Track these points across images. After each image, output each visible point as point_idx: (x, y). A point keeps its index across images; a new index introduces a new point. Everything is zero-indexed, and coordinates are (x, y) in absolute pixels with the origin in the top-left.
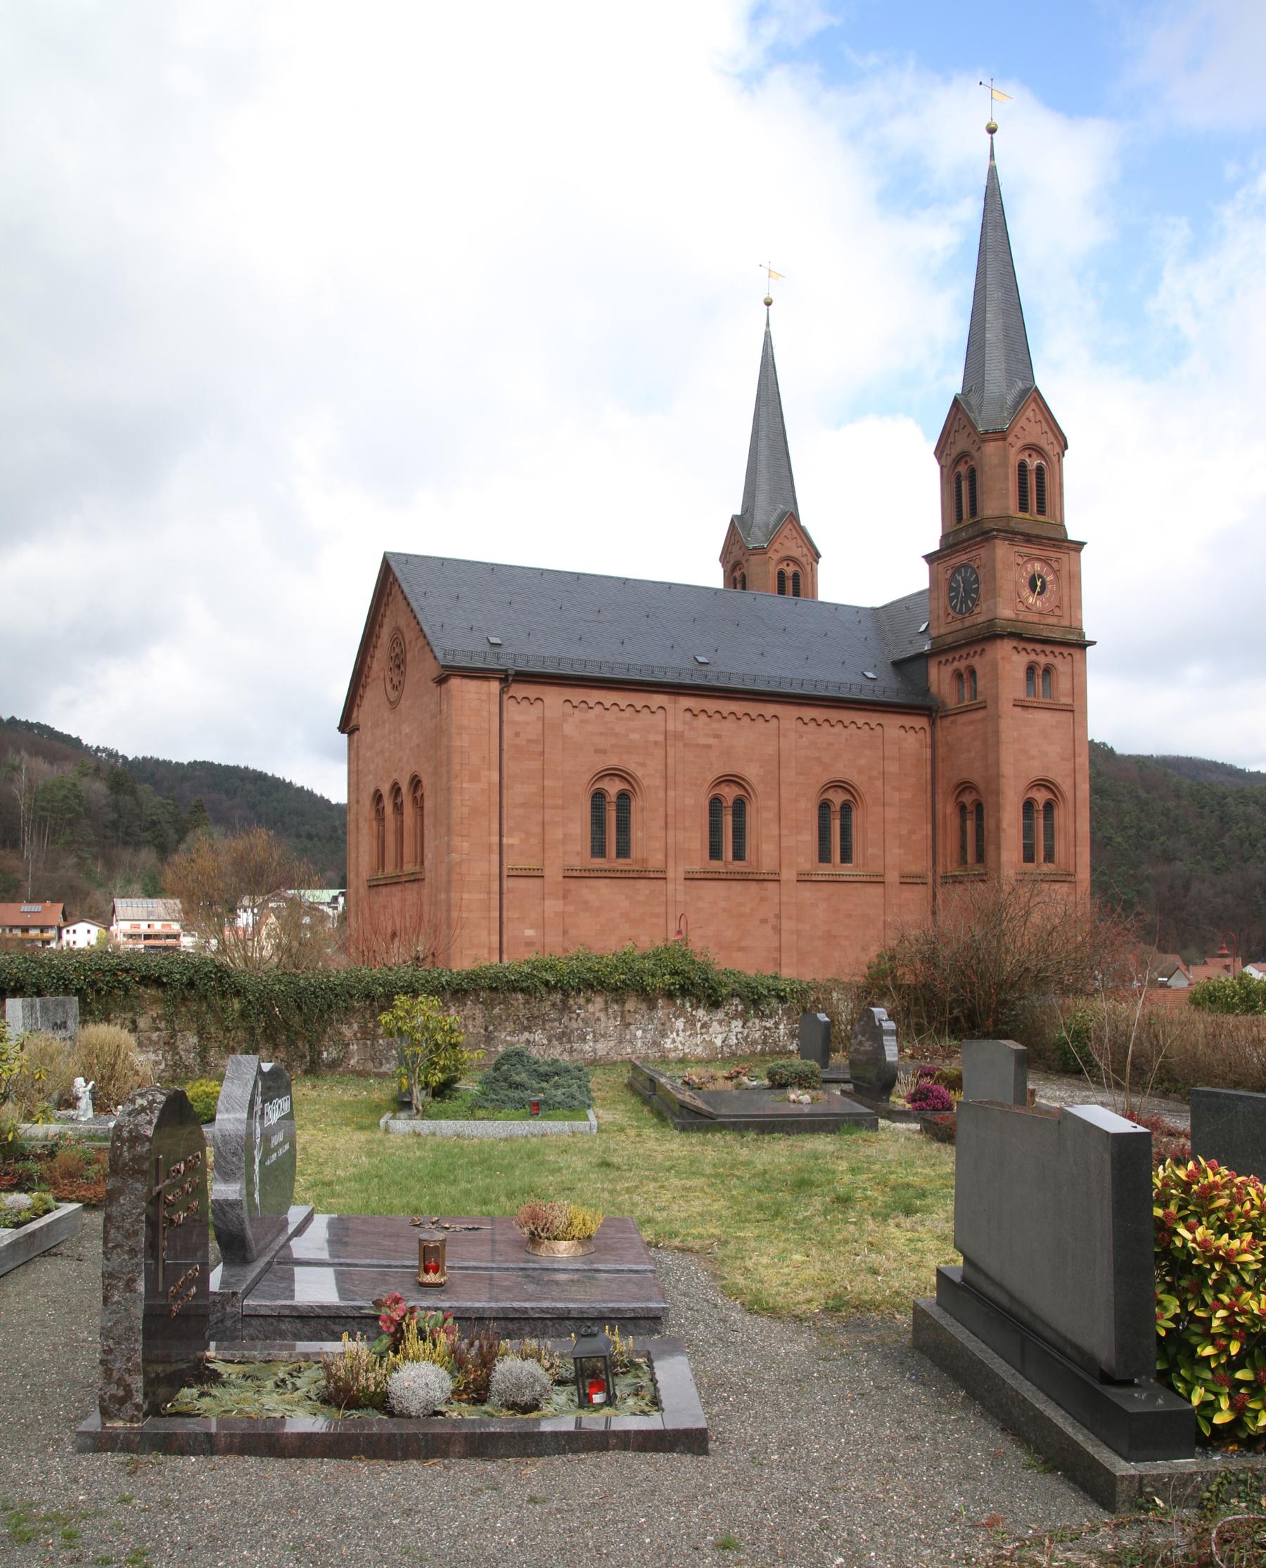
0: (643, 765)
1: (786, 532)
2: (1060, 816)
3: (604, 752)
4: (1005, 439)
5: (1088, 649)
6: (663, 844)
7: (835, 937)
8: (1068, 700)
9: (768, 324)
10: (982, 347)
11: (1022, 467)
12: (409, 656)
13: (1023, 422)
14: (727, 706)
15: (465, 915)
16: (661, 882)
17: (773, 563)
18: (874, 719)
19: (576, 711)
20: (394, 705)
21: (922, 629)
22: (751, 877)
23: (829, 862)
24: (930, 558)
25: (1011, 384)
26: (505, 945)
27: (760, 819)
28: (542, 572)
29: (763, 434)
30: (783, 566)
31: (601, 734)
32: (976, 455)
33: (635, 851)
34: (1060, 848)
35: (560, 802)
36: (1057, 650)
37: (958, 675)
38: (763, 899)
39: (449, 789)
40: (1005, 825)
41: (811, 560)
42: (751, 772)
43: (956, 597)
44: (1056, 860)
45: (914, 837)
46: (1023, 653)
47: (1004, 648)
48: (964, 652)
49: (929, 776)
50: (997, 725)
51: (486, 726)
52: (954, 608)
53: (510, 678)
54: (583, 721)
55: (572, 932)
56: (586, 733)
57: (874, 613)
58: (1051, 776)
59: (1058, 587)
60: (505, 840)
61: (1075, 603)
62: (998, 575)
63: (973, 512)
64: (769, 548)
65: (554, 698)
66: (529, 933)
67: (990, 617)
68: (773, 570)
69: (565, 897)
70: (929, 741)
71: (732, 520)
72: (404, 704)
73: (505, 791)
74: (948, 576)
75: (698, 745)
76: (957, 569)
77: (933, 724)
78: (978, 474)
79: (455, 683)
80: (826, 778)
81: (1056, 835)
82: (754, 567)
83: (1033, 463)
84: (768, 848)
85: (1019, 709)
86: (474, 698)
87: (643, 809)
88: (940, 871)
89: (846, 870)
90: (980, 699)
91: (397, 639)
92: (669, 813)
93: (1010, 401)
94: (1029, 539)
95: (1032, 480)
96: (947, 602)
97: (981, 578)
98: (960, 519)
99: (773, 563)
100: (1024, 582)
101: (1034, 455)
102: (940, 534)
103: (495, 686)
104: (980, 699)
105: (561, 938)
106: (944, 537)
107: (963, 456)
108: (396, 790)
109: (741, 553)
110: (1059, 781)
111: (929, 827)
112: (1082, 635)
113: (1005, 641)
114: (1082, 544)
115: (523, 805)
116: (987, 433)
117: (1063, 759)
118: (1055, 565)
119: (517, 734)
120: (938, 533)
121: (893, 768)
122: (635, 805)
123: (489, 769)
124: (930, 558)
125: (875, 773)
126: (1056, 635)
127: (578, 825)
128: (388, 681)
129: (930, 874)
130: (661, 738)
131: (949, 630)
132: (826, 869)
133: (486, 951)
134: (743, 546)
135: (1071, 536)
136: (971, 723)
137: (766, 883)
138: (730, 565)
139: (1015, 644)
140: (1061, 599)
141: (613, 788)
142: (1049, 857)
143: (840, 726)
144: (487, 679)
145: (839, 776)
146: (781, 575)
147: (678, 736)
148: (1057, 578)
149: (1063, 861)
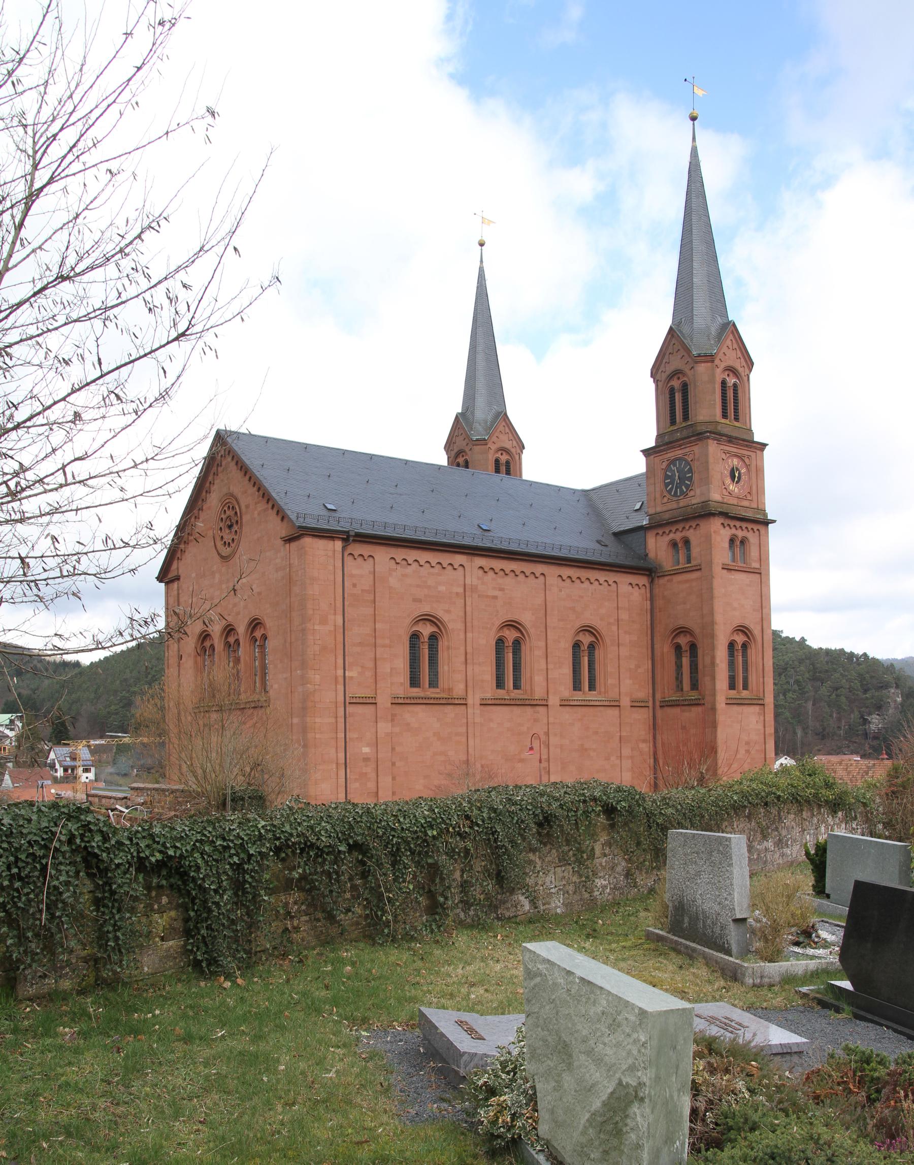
0: (448, 612)
1: (501, 428)
2: (752, 653)
3: (420, 601)
4: (713, 362)
6: (464, 676)
7: (586, 750)
8: (755, 565)
9: (482, 261)
10: (691, 287)
11: (724, 383)
12: (245, 518)
13: (724, 349)
14: (509, 566)
15: (317, 736)
16: (464, 707)
17: (492, 452)
18: (612, 577)
19: (399, 567)
21: (637, 507)
22: (527, 702)
24: (647, 452)
25: (713, 319)
26: (348, 761)
27: (533, 656)
28: (344, 452)
29: (480, 348)
31: (418, 586)
33: (443, 681)
35: (387, 642)
36: (750, 526)
37: (674, 544)
38: (536, 720)
39: (303, 630)
40: (718, 661)
41: (519, 451)
42: (526, 619)
44: (750, 687)
45: (639, 670)
46: (727, 528)
47: (716, 524)
48: (680, 526)
49: (649, 623)
50: (712, 584)
51: (332, 577)
52: (670, 492)
53: (351, 538)
56: (409, 586)
57: (586, 493)
58: (747, 623)
59: (750, 478)
60: (347, 674)
61: (760, 491)
63: (686, 417)
64: (483, 439)
65: (382, 555)
66: (366, 750)
67: (703, 499)
68: (491, 458)
70: (648, 595)
75: (487, 596)
76: (672, 462)
77: (652, 582)
78: (691, 389)
79: (307, 541)
80: (578, 624)
81: (750, 669)
82: (475, 455)
83: (731, 381)
84: (539, 679)
85: (725, 571)
86: (322, 554)
87: (448, 648)
88: (658, 696)
89: (592, 696)
90: (693, 563)
91: (230, 505)
93: (714, 330)
94: (731, 440)
95: (730, 394)
96: (663, 487)
97: (695, 469)
98: (673, 422)
99: (492, 452)
101: (731, 374)
102: (655, 434)
103: (339, 544)
104: (693, 563)
106: (659, 436)
107: (677, 373)
108: (229, 630)
109: (464, 443)
110: (752, 627)
111: (650, 662)
112: (765, 515)
113: (716, 518)
114: (765, 445)
115: (360, 644)
116: (699, 356)
117: (754, 610)
118: (747, 460)
119: (354, 585)
120: (654, 433)
121: (624, 616)
122: (442, 644)
123: (335, 614)
124: (647, 452)
125: (612, 620)
126: (749, 514)
127: (398, 662)
128: (218, 539)
129: (651, 699)
130: (461, 590)
131: (665, 509)
132: (578, 696)
133: (334, 766)
134: (468, 437)
136: (686, 581)
137: (538, 708)
138: (453, 453)
141: (426, 630)
142: (745, 687)
143: (587, 583)
144: (332, 538)
146: (497, 461)
147: (474, 589)
148: (748, 470)
149: (755, 689)
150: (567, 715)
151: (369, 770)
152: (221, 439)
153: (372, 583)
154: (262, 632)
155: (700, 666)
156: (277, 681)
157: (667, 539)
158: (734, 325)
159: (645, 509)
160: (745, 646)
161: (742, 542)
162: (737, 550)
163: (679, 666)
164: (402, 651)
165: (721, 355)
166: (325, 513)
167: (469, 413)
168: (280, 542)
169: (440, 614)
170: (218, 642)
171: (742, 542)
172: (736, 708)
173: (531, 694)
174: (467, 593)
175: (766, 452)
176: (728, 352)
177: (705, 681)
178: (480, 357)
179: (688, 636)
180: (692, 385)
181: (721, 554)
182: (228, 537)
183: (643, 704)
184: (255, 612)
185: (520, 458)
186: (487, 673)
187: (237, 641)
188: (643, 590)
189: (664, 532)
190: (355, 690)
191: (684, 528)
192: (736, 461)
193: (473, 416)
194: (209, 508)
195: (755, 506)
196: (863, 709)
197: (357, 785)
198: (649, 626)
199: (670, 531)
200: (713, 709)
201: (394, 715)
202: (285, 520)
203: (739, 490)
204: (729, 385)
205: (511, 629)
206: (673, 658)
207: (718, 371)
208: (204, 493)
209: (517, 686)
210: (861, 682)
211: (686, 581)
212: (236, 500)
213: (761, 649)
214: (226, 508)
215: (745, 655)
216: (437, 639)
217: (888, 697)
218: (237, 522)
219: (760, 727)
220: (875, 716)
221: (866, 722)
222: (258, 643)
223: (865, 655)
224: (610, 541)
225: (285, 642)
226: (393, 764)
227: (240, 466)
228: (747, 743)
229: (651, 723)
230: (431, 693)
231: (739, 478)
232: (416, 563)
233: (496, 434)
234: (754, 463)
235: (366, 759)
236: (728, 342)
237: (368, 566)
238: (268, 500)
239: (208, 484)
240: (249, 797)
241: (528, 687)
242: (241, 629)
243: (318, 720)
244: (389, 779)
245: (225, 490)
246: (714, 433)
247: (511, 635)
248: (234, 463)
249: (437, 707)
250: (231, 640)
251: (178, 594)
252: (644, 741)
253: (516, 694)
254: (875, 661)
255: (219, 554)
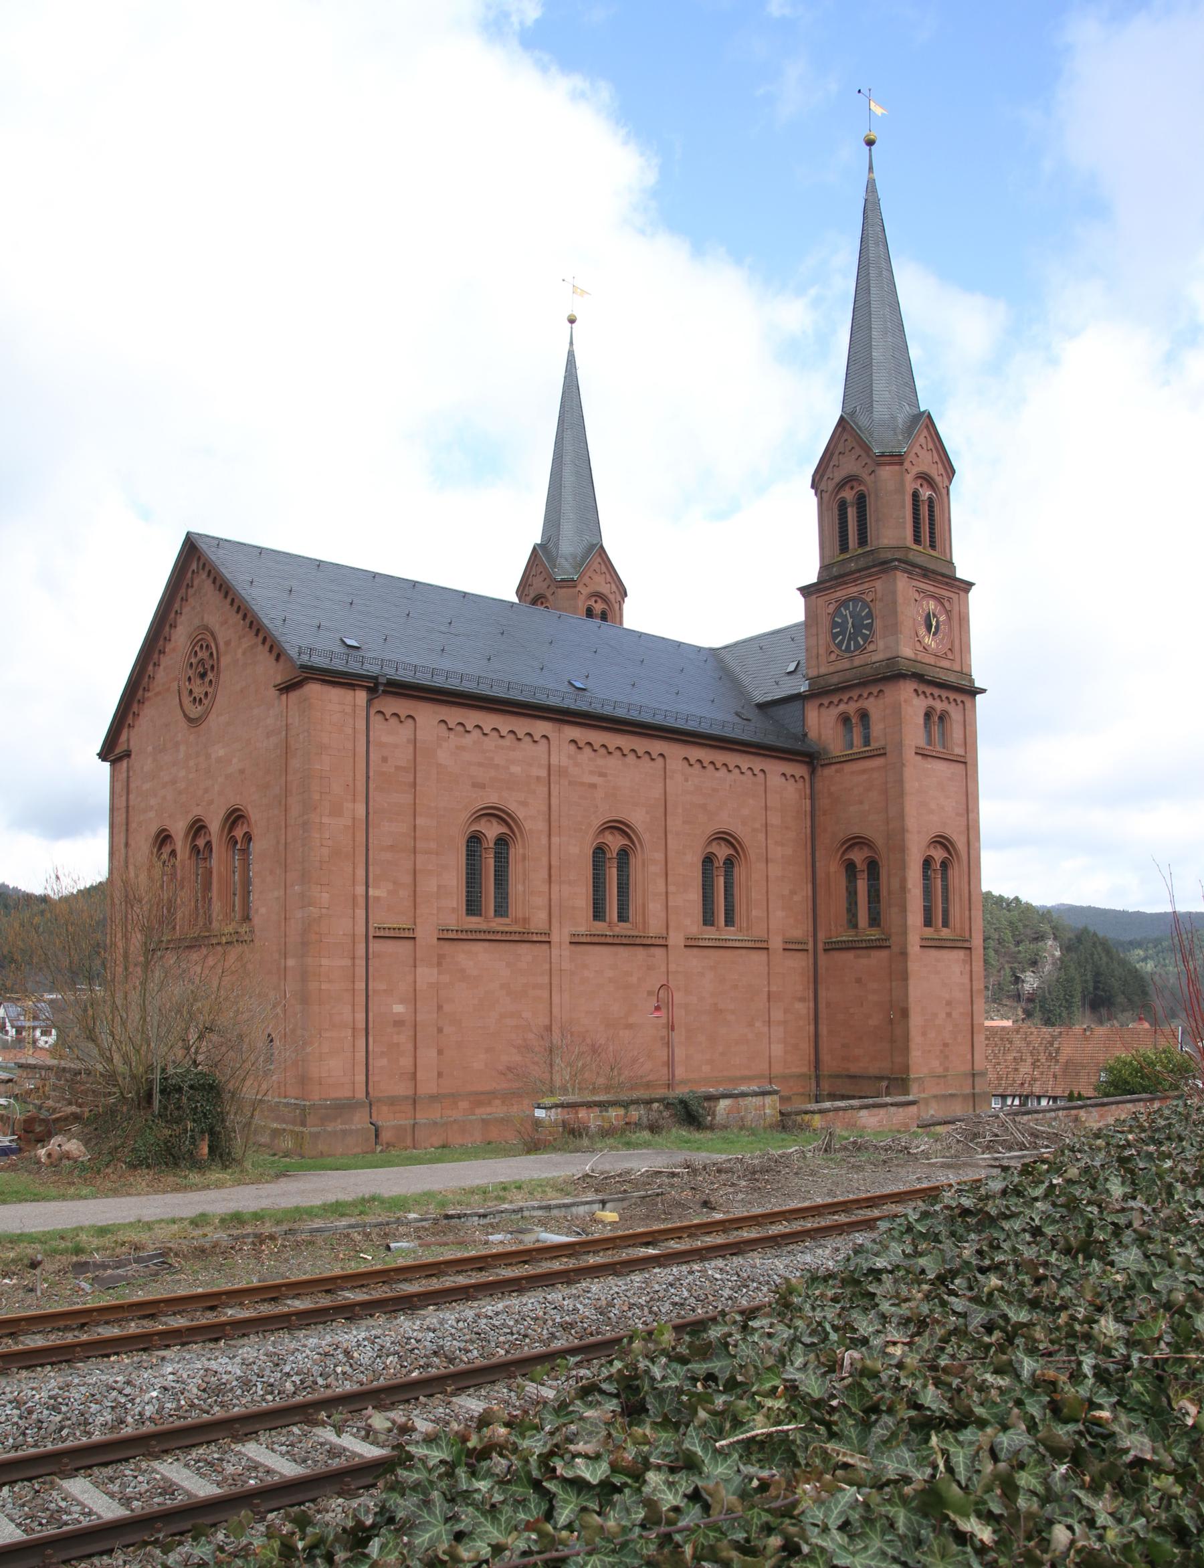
0: (524, 804)
1: (596, 566)
4: (901, 464)
5: (978, 697)
8: (959, 751)
9: (571, 343)
11: (915, 495)
12: (224, 661)
13: (917, 449)
16: (546, 946)
17: (582, 598)
20: (193, 722)
21: (791, 668)
22: (638, 941)
23: (712, 925)
24: (806, 591)
26: (371, 1025)
29: (567, 459)
30: (591, 602)
31: (480, 764)
32: (869, 479)
33: (517, 907)
34: (955, 911)
35: (433, 845)
37: (845, 719)
40: (910, 885)
41: (619, 598)
42: (637, 818)
43: (842, 633)
45: (796, 898)
46: (922, 697)
47: (907, 689)
48: (854, 694)
49: (809, 830)
50: (901, 774)
52: (839, 646)
54: (461, 748)
55: (447, 1008)
57: (713, 651)
59: (950, 627)
62: (899, 609)
63: (863, 540)
65: (428, 716)
66: (399, 1008)
67: (889, 655)
69: (439, 964)
70: (808, 791)
71: (534, 548)
72: (215, 721)
73: (371, 830)
74: (831, 611)
75: (582, 784)
76: (844, 603)
77: (813, 772)
81: (951, 896)
83: (925, 493)
84: (655, 908)
85: (919, 758)
86: (337, 708)
87: (524, 858)
88: (821, 936)
89: (730, 934)
90: (874, 745)
91: (204, 641)
92: (553, 863)
94: (927, 573)
97: (876, 612)
98: (844, 547)
99: (582, 598)
100: (921, 619)
101: (925, 485)
104: (874, 745)
105: (435, 1015)
106: (824, 568)
108: (198, 828)
109: (545, 585)
110: (955, 837)
111: (810, 886)
112: (972, 681)
114: (971, 584)
118: (947, 604)
119: (385, 760)
121: (774, 820)
123: (354, 801)
124: (806, 591)
125: (757, 825)
126: (952, 679)
127: (448, 877)
128: (185, 693)
129: (811, 939)
130: (544, 773)
131: (832, 669)
132: (710, 933)
133: (350, 1032)
135: (960, 574)
136: (864, 771)
139: (915, 686)
140: (952, 643)
141: (492, 831)
142: (946, 924)
143: (724, 770)
144: (352, 687)
145: (724, 827)
147: (563, 772)
148: (949, 618)
149: (958, 926)
150: (695, 961)
151: (403, 1038)
152: (194, 560)
153: (411, 757)
154: (245, 829)
155: (884, 893)
156: (264, 905)
157: (835, 712)
158: (929, 416)
159: (803, 669)
160: (945, 865)
161: (941, 718)
162: (936, 729)
163: (852, 893)
164: (457, 860)
165: (911, 456)
166: (343, 650)
167: (551, 545)
168: (273, 693)
169: (512, 807)
170: (180, 843)
171: (941, 718)
172: (934, 953)
173: (644, 927)
174: (552, 777)
175: (973, 594)
176: (922, 453)
177: (890, 915)
178: (568, 472)
179: (866, 849)
180: (872, 496)
181: (914, 734)
182: (198, 691)
183: (800, 947)
184: (234, 800)
185: (621, 609)
186: (580, 897)
187: (209, 844)
188: (800, 784)
189: (831, 703)
190: (381, 918)
191: (860, 696)
192: (932, 605)
193: (557, 549)
194: (174, 650)
195: (958, 668)
196: (1016, 965)
197: (384, 1062)
198: (809, 835)
199: (841, 700)
200: (904, 954)
201: (441, 957)
202: (282, 659)
203: (937, 645)
204: (922, 498)
205: (616, 832)
206: (842, 881)
207: (909, 478)
208: (167, 628)
209: (623, 917)
210: (1012, 931)
211: (864, 771)
212: (212, 634)
213: (966, 869)
214: (197, 649)
215: (945, 878)
216: (507, 844)
217: (1045, 951)
218: (213, 667)
219: (966, 980)
220: (1029, 974)
221: (1017, 980)
222: (238, 847)
223: (1017, 899)
224: (753, 714)
225: (278, 842)
226: (440, 1030)
227: (218, 584)
228: (949, 1003)
229: (811, 973)
230: (498, 924)
231: (937, 628)
232: (478, 731)
233: (588, 574)
234: (956, 608)
235: (398, 1023)
236: (922, 440)
237: (405, 731)
238: (258, 631)
239: (172, 615)
240: (191, 1087)
241: (639, 919)
242: (215, 826)
243: (324, 962)
244: (433, 1053)
245: (197, 622)
246: (905, 562)
247: (615, 842)
248: (210, 581)
249: (507, 945)
250: (201, 842)
251: (128, 777)
252: (802, 999)
253: (622, 928)
254: (1029, 908)
255: (185, 715)
